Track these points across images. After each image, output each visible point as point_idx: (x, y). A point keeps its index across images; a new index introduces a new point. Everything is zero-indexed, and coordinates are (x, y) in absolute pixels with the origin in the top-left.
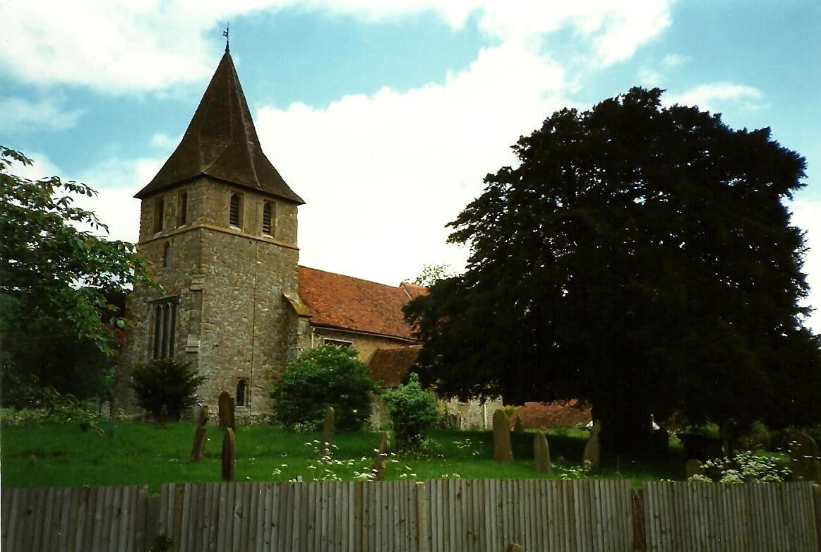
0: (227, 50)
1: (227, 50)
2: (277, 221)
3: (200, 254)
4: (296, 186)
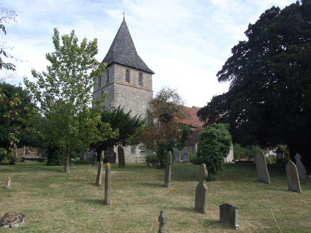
0: (124, 19)
1: (124, 19)
2: (144, 81)
3: (113, 93)
4: (151, 66)
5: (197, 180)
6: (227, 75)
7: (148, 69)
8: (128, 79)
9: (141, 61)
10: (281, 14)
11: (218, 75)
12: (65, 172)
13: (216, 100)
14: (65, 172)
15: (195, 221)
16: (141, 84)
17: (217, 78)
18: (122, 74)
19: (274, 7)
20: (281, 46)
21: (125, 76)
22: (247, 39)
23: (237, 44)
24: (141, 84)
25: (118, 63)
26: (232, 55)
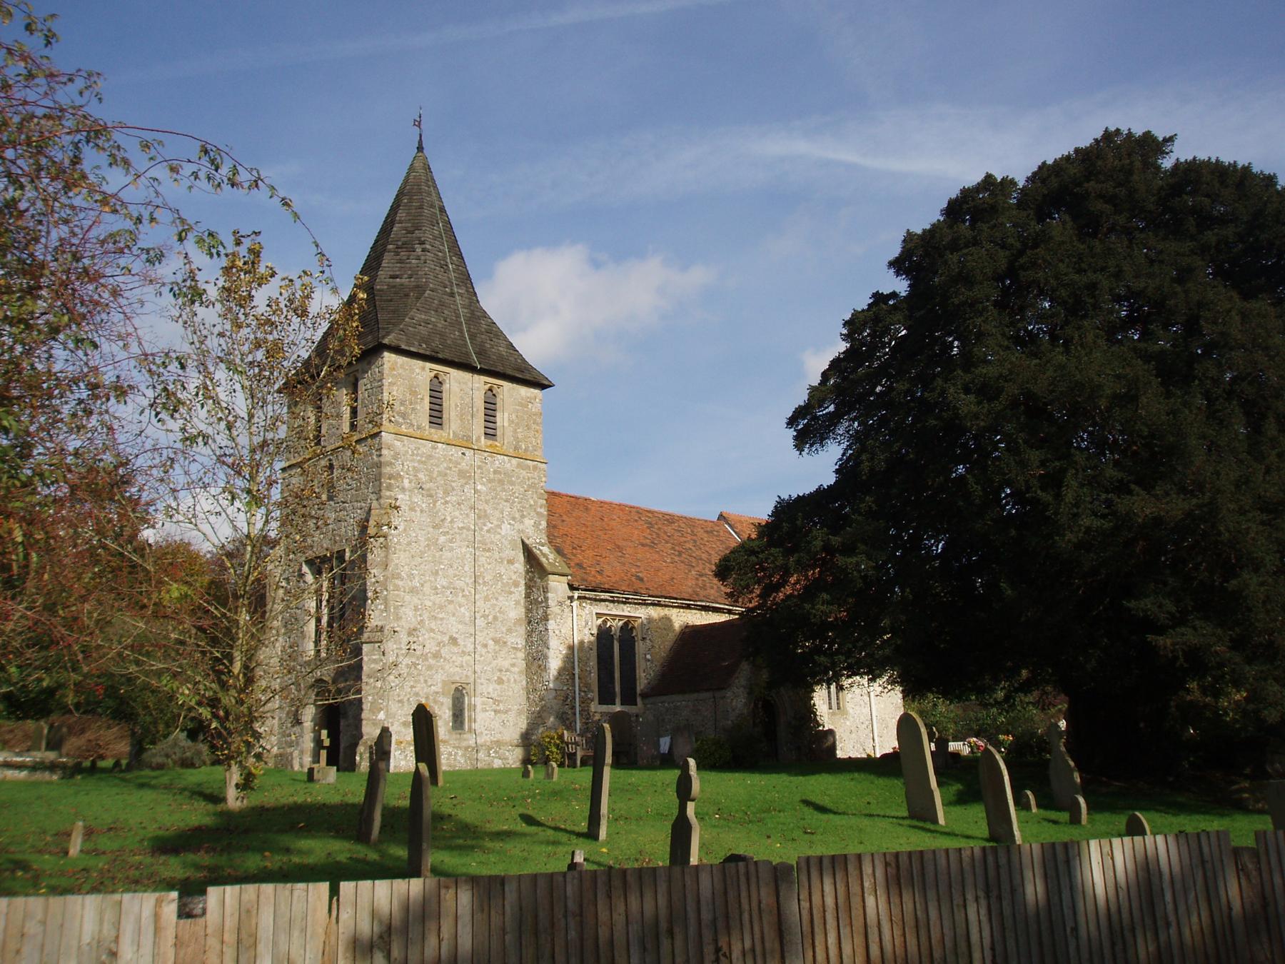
5: (946, 823)
6: (834, 419)
7: (529, 368)
8: (437, 417)
9: (494, 332)
10: (1021, 204)
11: (792, 422)
12: (1042, 844)
13: (787, 511)
14: (1042, 844)
15: (169, 760)
16: (490, 434)
17: (792, 433)
18: (414, 393)
19: (989, 177)
20: (954, 355)
21: (427, 399)
22: (901, 286)
23: (863, 302)
24: (490, 434)
25: (397, 350)
26: (843, 346)
